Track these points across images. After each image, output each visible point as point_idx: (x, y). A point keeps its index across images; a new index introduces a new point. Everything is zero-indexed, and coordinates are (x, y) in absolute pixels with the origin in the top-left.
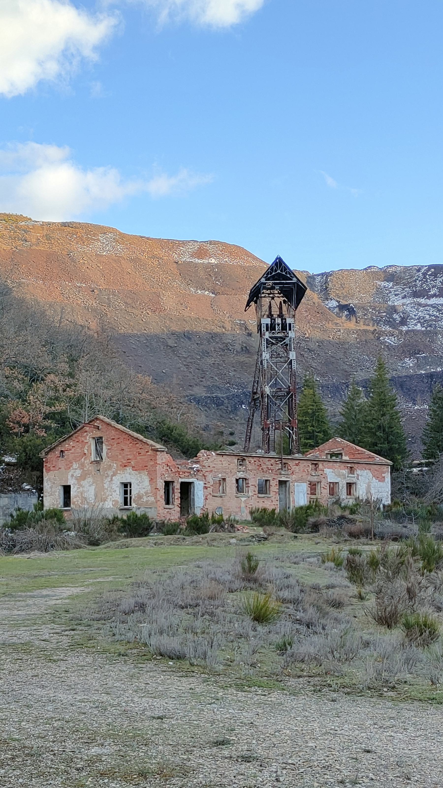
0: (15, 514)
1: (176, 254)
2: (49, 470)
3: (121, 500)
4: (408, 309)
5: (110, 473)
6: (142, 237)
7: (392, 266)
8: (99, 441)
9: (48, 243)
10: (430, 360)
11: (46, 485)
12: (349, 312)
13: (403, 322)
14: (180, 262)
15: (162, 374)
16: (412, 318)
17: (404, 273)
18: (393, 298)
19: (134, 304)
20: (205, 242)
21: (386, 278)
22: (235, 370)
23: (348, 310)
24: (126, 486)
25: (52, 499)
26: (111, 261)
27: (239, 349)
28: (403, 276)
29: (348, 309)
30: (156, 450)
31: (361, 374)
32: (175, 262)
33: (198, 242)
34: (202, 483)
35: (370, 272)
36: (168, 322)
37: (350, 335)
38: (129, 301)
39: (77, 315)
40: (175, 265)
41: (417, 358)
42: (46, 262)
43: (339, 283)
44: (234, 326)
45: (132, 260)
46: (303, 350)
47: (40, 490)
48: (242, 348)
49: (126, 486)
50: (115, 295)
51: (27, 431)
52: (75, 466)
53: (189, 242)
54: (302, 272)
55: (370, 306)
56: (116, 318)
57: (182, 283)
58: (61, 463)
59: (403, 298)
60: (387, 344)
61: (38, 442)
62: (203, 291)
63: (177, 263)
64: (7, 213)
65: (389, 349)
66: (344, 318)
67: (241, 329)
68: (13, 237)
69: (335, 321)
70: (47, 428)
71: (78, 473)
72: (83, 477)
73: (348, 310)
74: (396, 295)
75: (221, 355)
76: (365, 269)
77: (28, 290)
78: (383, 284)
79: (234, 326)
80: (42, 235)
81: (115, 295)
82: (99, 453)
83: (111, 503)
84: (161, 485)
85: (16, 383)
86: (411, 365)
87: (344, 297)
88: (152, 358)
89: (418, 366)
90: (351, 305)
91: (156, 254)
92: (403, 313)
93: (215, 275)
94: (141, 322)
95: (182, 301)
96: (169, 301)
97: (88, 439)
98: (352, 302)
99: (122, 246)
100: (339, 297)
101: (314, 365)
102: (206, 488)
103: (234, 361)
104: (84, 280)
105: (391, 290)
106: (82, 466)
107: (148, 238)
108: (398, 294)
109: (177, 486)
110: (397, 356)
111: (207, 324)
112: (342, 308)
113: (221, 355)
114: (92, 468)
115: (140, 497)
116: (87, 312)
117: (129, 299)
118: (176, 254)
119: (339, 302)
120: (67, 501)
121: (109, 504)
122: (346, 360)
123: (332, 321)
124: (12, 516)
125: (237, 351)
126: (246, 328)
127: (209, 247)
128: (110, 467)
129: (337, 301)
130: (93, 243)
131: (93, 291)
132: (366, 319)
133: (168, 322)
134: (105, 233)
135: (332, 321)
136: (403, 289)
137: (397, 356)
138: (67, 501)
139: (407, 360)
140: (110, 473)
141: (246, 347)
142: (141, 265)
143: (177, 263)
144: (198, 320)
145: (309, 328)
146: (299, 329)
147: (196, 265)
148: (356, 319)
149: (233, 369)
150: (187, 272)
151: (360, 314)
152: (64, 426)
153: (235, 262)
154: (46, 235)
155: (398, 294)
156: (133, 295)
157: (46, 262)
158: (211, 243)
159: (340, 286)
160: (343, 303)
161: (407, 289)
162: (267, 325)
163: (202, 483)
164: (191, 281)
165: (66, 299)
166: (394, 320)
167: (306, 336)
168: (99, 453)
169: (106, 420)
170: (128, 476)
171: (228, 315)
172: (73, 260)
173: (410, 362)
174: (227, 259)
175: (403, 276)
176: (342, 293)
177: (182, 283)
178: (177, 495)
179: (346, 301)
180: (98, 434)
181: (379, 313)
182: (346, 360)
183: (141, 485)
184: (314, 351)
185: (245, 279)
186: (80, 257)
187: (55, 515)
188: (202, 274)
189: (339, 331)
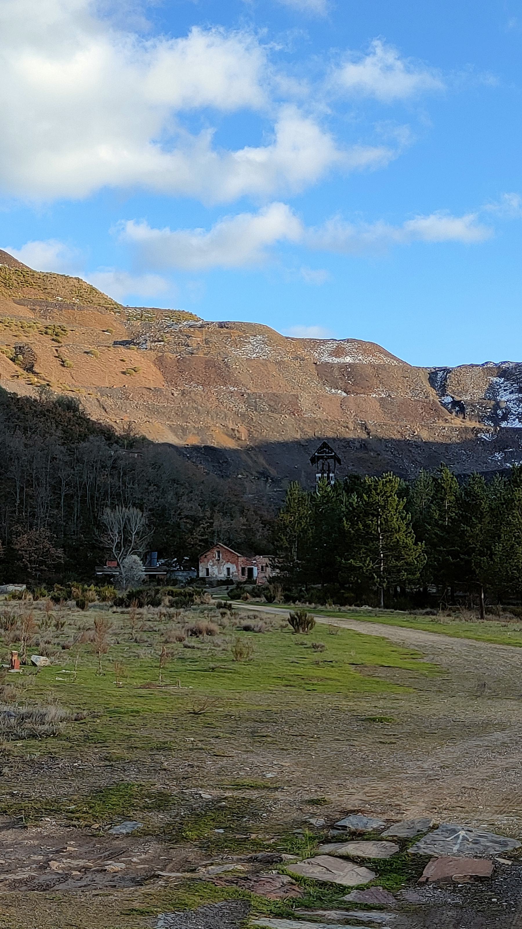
0: (189, 579)
1: (317, 352)
2: (201, 562)
3: (226, 574)
4: (511, 405)
5: (223, 564)
6: (287, 338)
7: (506, 362)
8: (219, 552)
9: (207, 347)
10: (515, 454)
11: (200, 568)
12: (460, 408)
13: (505, 418)
14: (318, 363)
15: (295, 469)
16: (513, 414)
17: (515, 368)
18: (502, 393)
19: (276, 406)
20: (342, 340)
21: (499, 374)
22: (353, 465)
23: (459, 407)
24: (228, 569)
25: (202, 574)
26: (259, 365)
27: (358, 447)
28: (513, 372)
29: (459, 405)
30: (238, 556)
31: (458, 466)
32: (314, 363)
33: (336, 340)
34: (256, 568)
35: (487, 369)
36: (302, 424)
37: (453, 432)
38: (272, 403)
39: (229, 420)
40: (314, 365)
41: (505, 453)
42: (205, 368)
43: (456, 379)
44: (356, 426)
45: (278, 363)
46: (411, 447)
47: (198, 570)
48: (361, 445)
49: (228, 569)
50: (261, 399)
51: (193, 547)
52: (211, 561)
53: (329, 340)
54: (426, 368)
55: (478, 403)
56: (260, 422)
57: (319, 383)
58: (206, 560)
59: (510, 393)
60: (483, 440)
61: (197, 551)
62: (336, 390)
63: (316, 364)
64: (171, 309)
65: (484, 445)
66: (454, 413)
67: (362, 429)
68: (177, 342)
69: (446, 417)
70: (200, 546)
71: (212, 564)
72: (213, 565)
73: (459, 407)
74: (505, 390)
75: (343, 452)
76: (483, 365)
77: (191, 397)
78: (495, 379)
79: (356, 426)
80: (201, 339)
81: (261, 399)
82: (219, 556)
83: (223, 575)
84: (240, 568)
85: (188, 525)
86: (499, 458)
87: (458, 393)
88: (287, 456)
89: (506, 459)
90: (462, 402)
91: (299, 354)
92: (506, 409)
93: (347, 374)
94: (280, 424)
95: (316, 402)
96: (305, 402)
97: (215, 551)
98: (465, 398)
99: (270, 348)
100: (454, 394)
101: (419, 459)
102: (258, 569)
103: (353, 458)
104: (236, 385)
105: (502, 385)
106: (213, 561)
107: (292, 339)
108: (507, 390)
109: (246, 569)
110: (489, 450)
111: (334, 425)
112: (455, 403)
113: (343, 452)
114: (216, 562)
115: (233, 573)
116: (236, 417)
117: (272, 402)
118: (317, 352)
119: (453, 398)
120: (208, 574)
121: (222, 575)
122: (447, 454)
123: (443, 417)
124: (188, 579)
125: (357, 448)
126: (366, 428)
127: (347, 345)
128: (223, 562)
129: (452, 397)
130: (245, 345)
131: (243, 395)
132: (472, 415)
133: (302, 424)
134: (255, 336)
135: (443, 417)
136: (512, 385)
137: (489, 450)
138: (208, 574)
139: (496, 454)
140: (223, 564)
141: (364, 444)
142: (285, 367)
143: (316, 364)
144: (326, 421)
145: (419, 427)
146: (410, 428)
147: (332, 366)
148: (464, 415)
149: (351, 464)
150: (324, 372)
151: (468, 410)
152: (207, 546)
153: (371, 359)
154: (205, 339)
155: (507, 390)
156: (276, 398)
157: (205, 368)
158: (348, 341)
159: (456, 382)
160: (457, 399)
161: (515, 385)
162: (319, 477)
163: (256, 568)
164: (327, 381)
165: (220, 404)
166: (498, 415)
167: (415, 434)
168: (219, 556)
169: (222, 545)
170: (229, 565)
171: (354, 414)
172: (227, 366)
173: (498, 456)
174: (361, 358)
175: (513, 372)
176: (458, 389)
177: (319, 383)
178: (247, 572)
179: (460, 397)
180: (219, 550)
181: (485, 409)
182: (447, 454)
183: (233, 568)
184: (420, 447)
185: (373, 378)
186: (233, 362)
187: (203, 579)
188: (336, 373)
189: (444, 429)
